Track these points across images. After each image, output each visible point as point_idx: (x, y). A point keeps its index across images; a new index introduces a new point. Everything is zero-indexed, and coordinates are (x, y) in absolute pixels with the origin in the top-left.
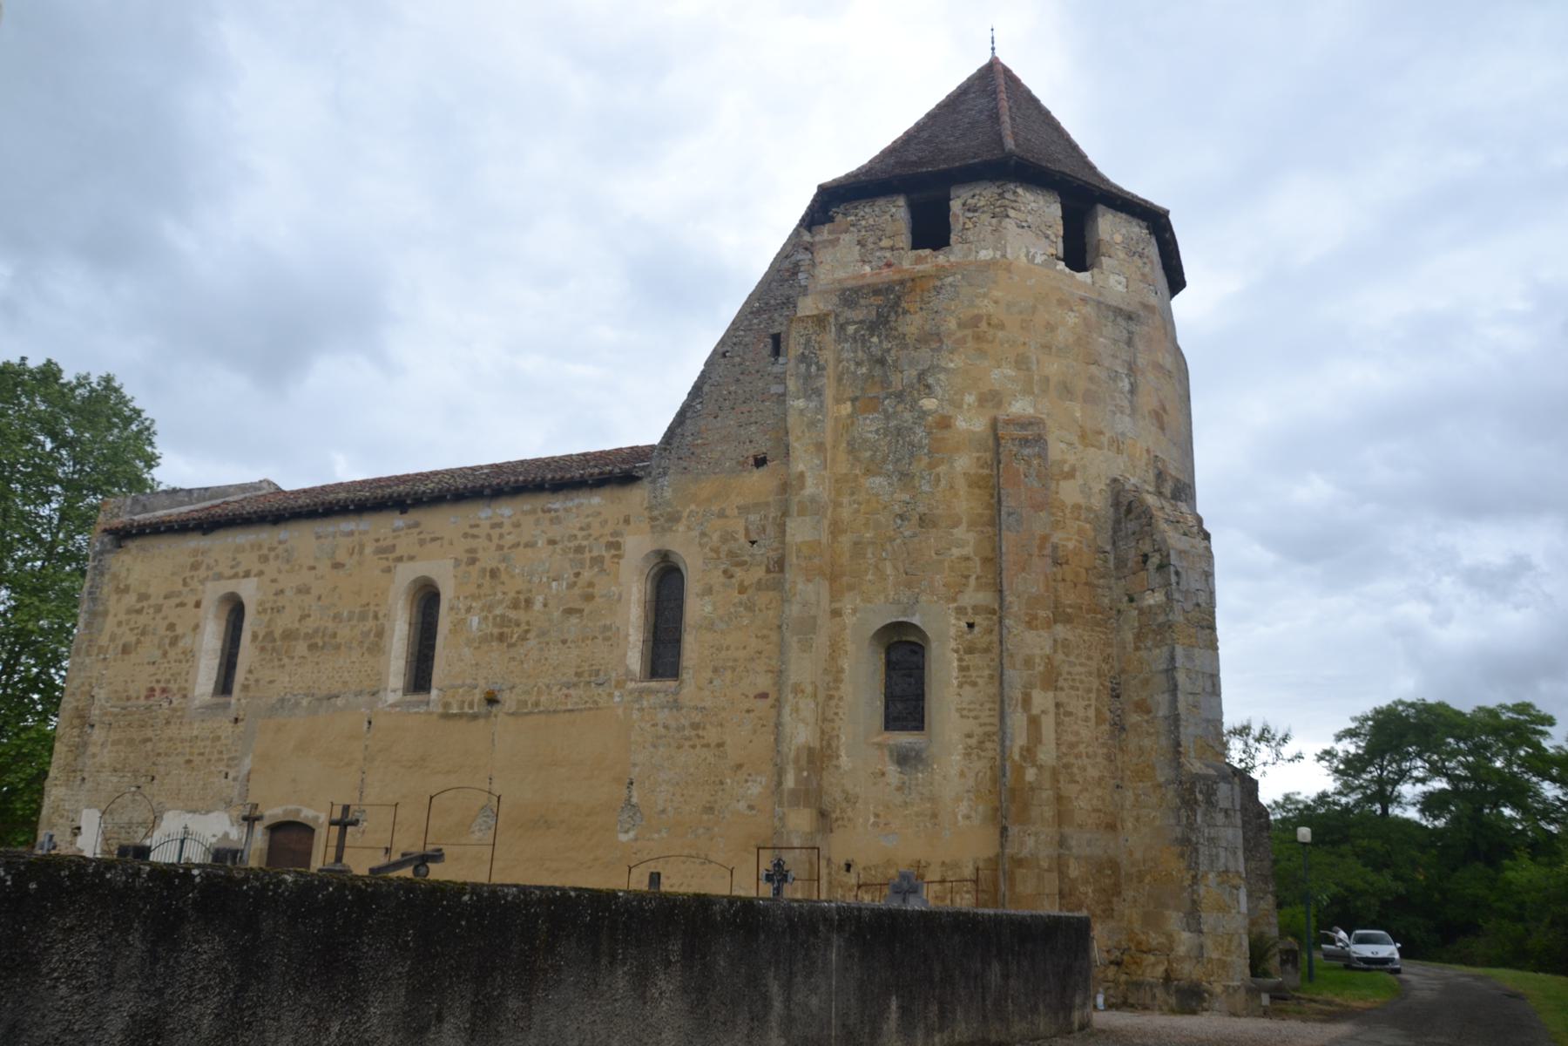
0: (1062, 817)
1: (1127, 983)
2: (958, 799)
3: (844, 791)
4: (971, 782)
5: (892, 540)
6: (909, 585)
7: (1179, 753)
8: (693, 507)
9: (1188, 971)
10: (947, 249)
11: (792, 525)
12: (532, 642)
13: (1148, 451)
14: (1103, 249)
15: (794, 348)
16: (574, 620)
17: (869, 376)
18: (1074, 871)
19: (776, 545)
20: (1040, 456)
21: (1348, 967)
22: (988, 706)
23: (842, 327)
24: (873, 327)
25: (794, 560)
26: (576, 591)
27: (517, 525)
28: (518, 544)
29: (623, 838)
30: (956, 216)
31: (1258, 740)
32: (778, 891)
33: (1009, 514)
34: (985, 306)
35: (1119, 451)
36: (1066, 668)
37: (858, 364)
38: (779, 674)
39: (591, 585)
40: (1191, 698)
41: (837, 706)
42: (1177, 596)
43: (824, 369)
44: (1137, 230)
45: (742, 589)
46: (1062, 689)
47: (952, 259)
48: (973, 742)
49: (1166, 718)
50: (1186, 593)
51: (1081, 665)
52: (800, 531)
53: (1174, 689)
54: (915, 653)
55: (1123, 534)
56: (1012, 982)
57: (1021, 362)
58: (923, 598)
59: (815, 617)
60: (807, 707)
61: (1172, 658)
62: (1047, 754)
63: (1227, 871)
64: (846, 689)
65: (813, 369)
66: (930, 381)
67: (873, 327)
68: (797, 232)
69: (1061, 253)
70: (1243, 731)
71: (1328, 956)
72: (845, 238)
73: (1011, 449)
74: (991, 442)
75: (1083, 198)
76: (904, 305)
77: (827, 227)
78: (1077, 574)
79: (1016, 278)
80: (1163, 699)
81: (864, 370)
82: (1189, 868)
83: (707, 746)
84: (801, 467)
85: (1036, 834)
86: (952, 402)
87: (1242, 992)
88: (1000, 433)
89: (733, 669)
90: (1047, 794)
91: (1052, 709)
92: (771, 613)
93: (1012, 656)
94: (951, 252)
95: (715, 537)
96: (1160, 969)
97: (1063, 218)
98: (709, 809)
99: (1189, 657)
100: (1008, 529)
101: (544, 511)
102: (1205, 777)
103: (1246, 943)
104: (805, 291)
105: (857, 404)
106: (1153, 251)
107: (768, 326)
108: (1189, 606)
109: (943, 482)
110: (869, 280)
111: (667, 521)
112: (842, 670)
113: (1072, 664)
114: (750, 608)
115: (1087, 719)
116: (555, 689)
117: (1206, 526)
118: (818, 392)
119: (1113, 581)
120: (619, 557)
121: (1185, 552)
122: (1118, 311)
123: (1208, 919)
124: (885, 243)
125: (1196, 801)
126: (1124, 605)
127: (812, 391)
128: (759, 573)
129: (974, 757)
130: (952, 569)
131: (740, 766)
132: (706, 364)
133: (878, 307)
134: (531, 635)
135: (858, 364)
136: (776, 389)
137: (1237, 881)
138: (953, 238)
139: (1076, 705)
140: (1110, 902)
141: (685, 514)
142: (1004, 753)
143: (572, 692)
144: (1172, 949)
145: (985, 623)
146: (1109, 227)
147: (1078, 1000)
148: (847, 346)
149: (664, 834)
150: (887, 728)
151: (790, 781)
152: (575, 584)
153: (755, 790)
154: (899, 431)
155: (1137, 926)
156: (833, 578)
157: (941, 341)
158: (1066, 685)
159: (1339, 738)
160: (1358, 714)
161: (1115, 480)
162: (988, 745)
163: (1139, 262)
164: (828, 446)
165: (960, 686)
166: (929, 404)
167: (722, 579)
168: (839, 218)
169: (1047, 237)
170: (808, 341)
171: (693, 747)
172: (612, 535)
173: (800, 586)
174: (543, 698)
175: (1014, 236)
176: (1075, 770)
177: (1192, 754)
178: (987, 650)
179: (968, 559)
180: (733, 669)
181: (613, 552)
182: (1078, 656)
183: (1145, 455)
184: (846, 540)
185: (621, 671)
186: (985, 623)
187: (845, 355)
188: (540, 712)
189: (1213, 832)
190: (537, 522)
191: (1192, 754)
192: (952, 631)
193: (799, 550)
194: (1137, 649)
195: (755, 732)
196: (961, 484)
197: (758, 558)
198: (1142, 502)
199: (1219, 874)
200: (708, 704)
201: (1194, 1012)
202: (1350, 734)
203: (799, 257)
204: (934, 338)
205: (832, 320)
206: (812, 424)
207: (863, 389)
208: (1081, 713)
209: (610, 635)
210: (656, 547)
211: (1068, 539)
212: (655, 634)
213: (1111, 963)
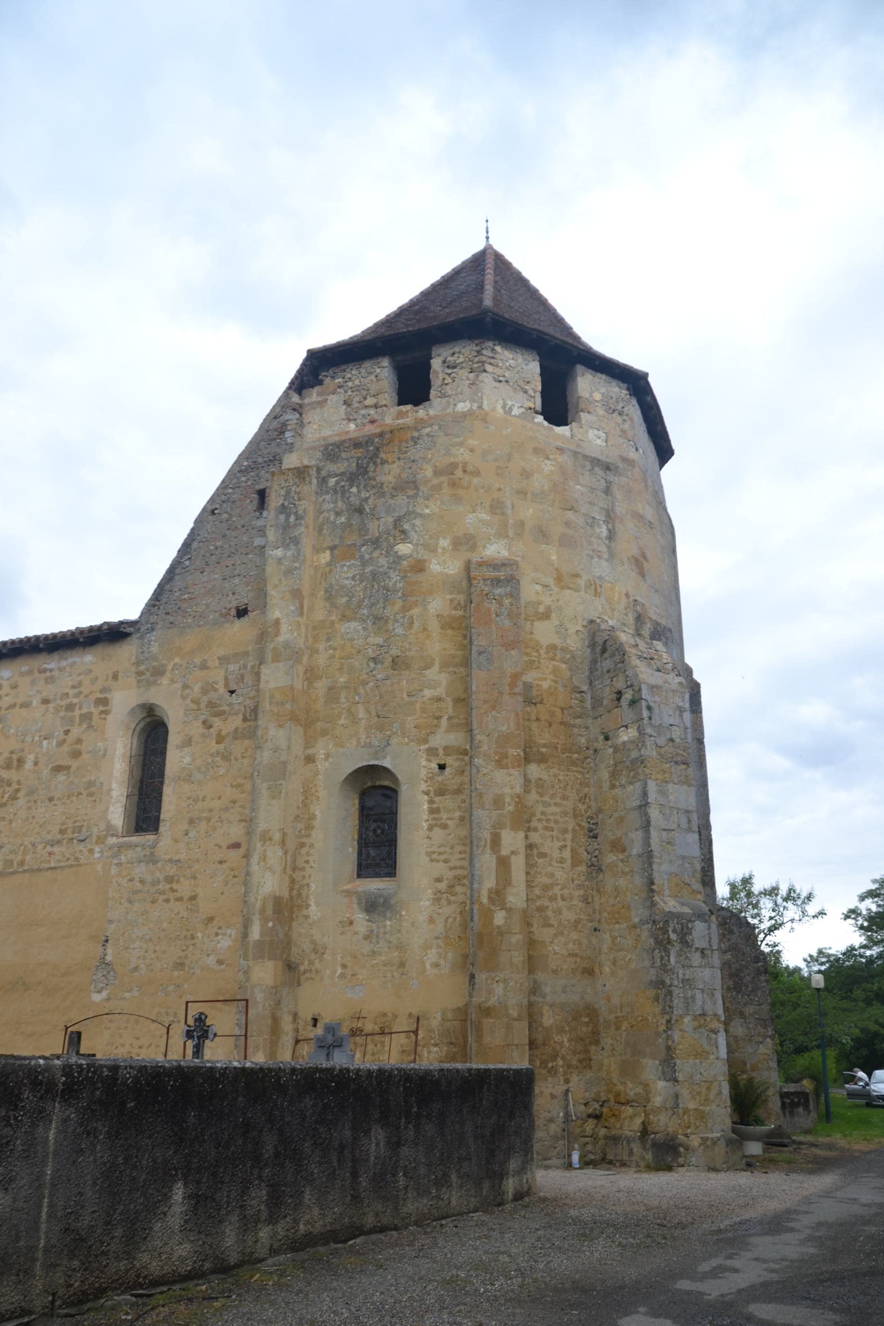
0: (532, 963)
1: (606, 1137)
2: (427, 947)
3: (313, 942)
4: (440, 928)
5: (365, 683)
6: (380, 728)
7: (652, 891)
8: (177, 660)
9: (665, 1123)
10: (427, 403)
11: (265, 671)
12: (22, 802)
13: (627, 595)
14: (582, 406)
15: (274, 501)
16: (61, 777)
17: (348, 525)
18: (548, 1019)
19: (252, 694)
20: (511, 595)
21: (869, 1105)
22: (458, 848)
23: (323, 481)
24: (352, 478)
25: (267, 707)
26: (66, 748)
27: (14, 687)
28: (14, 705)
29: (96, 998)
30: (436, 372)
31: (786, 899)
32: (198, 1051)
33: (480, 653)
34: (461, 455)
35: (597, 594)
36: (540, 808)
37: (338, 514)
38: (249, 822)
39: (79, 741)
40: (664, 834)
41: (308, 854)
42: (649, 730)
43: (302, 518)
44: (617, 390)
45: (220, 739)
46: (536, 830)
47: (432, 412)
48: (443, 886)
49: (640, 856)
50: (659, 728)
51: (555, 804)
52: (274, 677)
53: (647, 825)
54: (388, 797)
55: (598, 673)
56: (405, 1151)
57: (496, 507)
58: (394, 741)
59: (285, 764)
60: (275, 854)
61: (645, 794)
62: (516, 897)
63: (703, 1015)
64: (317, 835)
65: (292, 519)
66: (406, 526)
67: (352, 478)
68: (286, 394)
69: (539, 406)
70: (772, 892)
71: (852, 1095)
72: (333, 398)
73: (486, 589)
74: (464, 584)
75: (562, 362)
76: (382, 455)
77: (317, 389)
78: (552, 714)
79: (492, 428)
80: (637, 836)
81: (343, 519)
82: (664, 1012)
83: (179, 899)
84: (277, 614)
85: (505, 981)
86: (426, 547)
87: (722, 1144)
88: (473, 574)
89: (208, 820)
90: (517, 938)
91: (522, 850)
92: (246, 761)
93: (480, 796)
94: (431, 406)
95: (197, 688)
96: (638, 1121)
97: (542, 374)
98: (180, 965)
99: (663, 793)
100: (479, 668)
101: (40, 672)
102: (679, 916)
103: (726, 1090)
104: (291, 448)
105: (336, 552)
106: (634, 411)
107: (254, 486)
108: (661, 741)
109: (416, 624)
110: (352, 436)
111: (153, 675)
112: (313, 817)
113: (546, 804)
114: (226, 758)
115: (562, 861)
116: (41, 847)
117: (696, 676)
118: (296, 541)
119: (590, 721)
120: (106, 712)
121: (657, 687)
122: (595, 462)
123: (684, 1067)
124: (370, 401)
125: (669, 942)
126: (600, 744)
127: (291, 540)
128: (236, 722)
129: (444, 902)
130: (423, 710)
131: (211, 919)
132: (196, 522)
133: (359, 458)
134: (21, 794)
135: (338, 514)
136: (258, 541)
137: (715, 1025)
138: (433, 393)
139: (551, 847)
140: (587, 1051)
141: (170, 667)
142: (473, 898)
143: (56, 849)
144: (648, 1100)
145: (456, 764)
146: (587, 386)
147: (513, 1165)
148: (328, 497)
149: (136, 994)
150: (359, 876)
151: (255, 933)
152: (64, 741)
153: (225, 943)
154: (374, 576)
155: (615, 1077)
156: (307, 725)
157: (417, 488)
158: (539, 826)
159: (862, 898)
160: (878, 877)
161: (592, 622)
162: (458, 889)
163: (619, 419)
164: (306, 593)
165: (430, 828)
166: (404, 549)
167: (202, 730)
168: (327, 381)
169: (526, 392)
170: (288, 493)
171: (167, 901)
172: (101, 691)
173: (272, 732)
174: (28, 858)
175: (495, 389)
176: (550, 913)
177: (667, 892)
178: (458, 791)
179: (439, 699)
180: (208, 820)
181: (101, 708)
182: (553, 796)
183: (624, 598)
184: (321, 686)
185: (102, 826)
186: (456, 764)
187: (326, 506)
188: (25, 871)
189: (688, 974)
190: (33, 683)
191: (667, 892)
192: (423, 773)
193: (272, 697)
194: (613, 787)
195: (226, 883)
196: (434, 626)
197: (236, 707)
198: (615, 639)
199: (695, 1018)
200: (183, 856)
201: (669, 1169)
202: (871, 894)
203: (287, 417)
204: (409, 485)
205: (313, 472)
206: (289, 572)
207: (341, 537)
208: (556, 854)
209: (94, 791)
210: (141, 701)
211: (542, 679)
212: (141, 789)
213: (589, 1116)
